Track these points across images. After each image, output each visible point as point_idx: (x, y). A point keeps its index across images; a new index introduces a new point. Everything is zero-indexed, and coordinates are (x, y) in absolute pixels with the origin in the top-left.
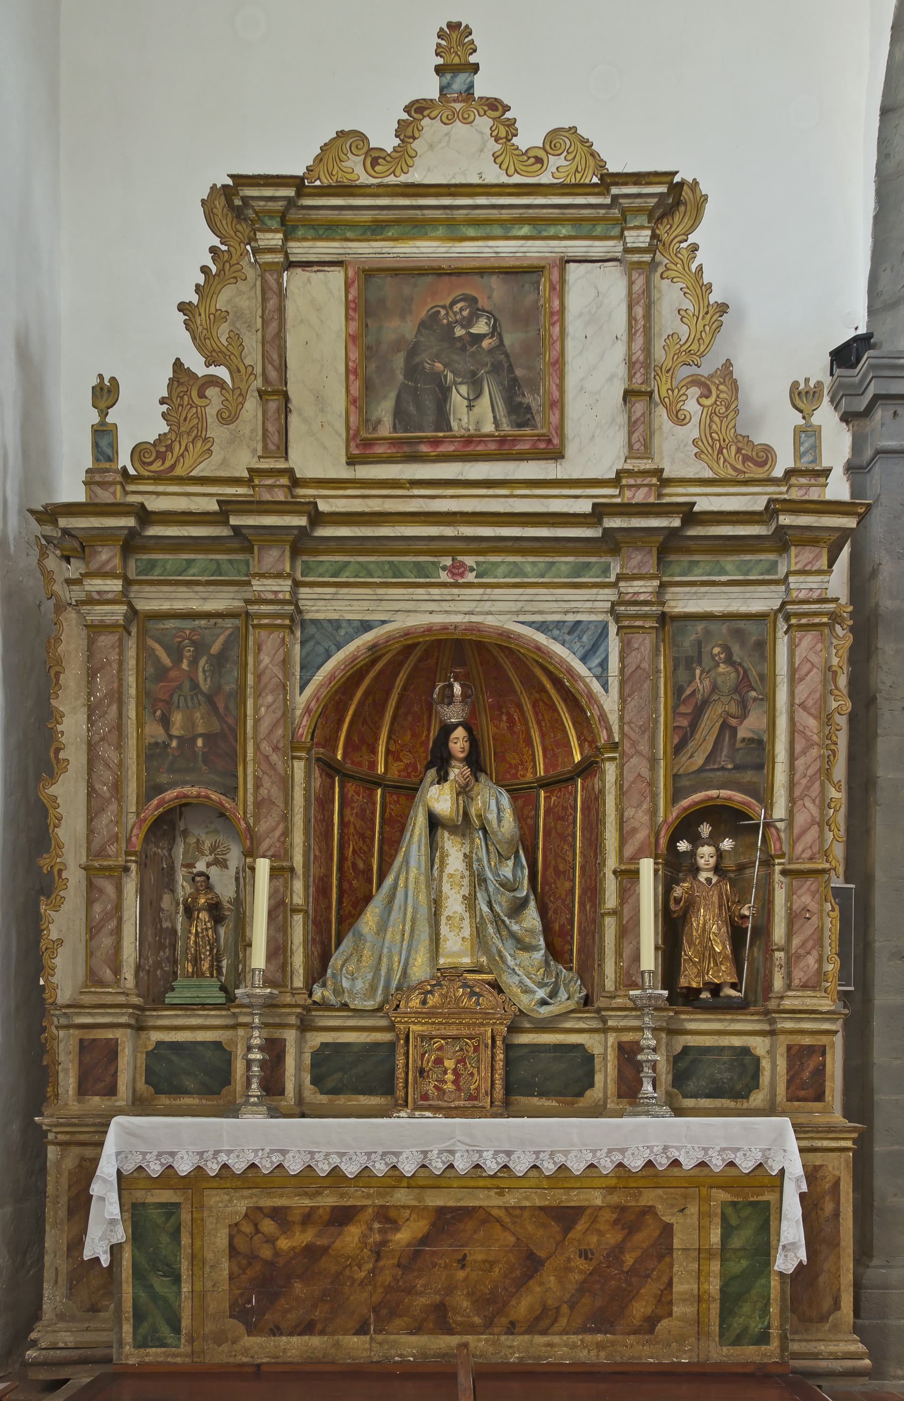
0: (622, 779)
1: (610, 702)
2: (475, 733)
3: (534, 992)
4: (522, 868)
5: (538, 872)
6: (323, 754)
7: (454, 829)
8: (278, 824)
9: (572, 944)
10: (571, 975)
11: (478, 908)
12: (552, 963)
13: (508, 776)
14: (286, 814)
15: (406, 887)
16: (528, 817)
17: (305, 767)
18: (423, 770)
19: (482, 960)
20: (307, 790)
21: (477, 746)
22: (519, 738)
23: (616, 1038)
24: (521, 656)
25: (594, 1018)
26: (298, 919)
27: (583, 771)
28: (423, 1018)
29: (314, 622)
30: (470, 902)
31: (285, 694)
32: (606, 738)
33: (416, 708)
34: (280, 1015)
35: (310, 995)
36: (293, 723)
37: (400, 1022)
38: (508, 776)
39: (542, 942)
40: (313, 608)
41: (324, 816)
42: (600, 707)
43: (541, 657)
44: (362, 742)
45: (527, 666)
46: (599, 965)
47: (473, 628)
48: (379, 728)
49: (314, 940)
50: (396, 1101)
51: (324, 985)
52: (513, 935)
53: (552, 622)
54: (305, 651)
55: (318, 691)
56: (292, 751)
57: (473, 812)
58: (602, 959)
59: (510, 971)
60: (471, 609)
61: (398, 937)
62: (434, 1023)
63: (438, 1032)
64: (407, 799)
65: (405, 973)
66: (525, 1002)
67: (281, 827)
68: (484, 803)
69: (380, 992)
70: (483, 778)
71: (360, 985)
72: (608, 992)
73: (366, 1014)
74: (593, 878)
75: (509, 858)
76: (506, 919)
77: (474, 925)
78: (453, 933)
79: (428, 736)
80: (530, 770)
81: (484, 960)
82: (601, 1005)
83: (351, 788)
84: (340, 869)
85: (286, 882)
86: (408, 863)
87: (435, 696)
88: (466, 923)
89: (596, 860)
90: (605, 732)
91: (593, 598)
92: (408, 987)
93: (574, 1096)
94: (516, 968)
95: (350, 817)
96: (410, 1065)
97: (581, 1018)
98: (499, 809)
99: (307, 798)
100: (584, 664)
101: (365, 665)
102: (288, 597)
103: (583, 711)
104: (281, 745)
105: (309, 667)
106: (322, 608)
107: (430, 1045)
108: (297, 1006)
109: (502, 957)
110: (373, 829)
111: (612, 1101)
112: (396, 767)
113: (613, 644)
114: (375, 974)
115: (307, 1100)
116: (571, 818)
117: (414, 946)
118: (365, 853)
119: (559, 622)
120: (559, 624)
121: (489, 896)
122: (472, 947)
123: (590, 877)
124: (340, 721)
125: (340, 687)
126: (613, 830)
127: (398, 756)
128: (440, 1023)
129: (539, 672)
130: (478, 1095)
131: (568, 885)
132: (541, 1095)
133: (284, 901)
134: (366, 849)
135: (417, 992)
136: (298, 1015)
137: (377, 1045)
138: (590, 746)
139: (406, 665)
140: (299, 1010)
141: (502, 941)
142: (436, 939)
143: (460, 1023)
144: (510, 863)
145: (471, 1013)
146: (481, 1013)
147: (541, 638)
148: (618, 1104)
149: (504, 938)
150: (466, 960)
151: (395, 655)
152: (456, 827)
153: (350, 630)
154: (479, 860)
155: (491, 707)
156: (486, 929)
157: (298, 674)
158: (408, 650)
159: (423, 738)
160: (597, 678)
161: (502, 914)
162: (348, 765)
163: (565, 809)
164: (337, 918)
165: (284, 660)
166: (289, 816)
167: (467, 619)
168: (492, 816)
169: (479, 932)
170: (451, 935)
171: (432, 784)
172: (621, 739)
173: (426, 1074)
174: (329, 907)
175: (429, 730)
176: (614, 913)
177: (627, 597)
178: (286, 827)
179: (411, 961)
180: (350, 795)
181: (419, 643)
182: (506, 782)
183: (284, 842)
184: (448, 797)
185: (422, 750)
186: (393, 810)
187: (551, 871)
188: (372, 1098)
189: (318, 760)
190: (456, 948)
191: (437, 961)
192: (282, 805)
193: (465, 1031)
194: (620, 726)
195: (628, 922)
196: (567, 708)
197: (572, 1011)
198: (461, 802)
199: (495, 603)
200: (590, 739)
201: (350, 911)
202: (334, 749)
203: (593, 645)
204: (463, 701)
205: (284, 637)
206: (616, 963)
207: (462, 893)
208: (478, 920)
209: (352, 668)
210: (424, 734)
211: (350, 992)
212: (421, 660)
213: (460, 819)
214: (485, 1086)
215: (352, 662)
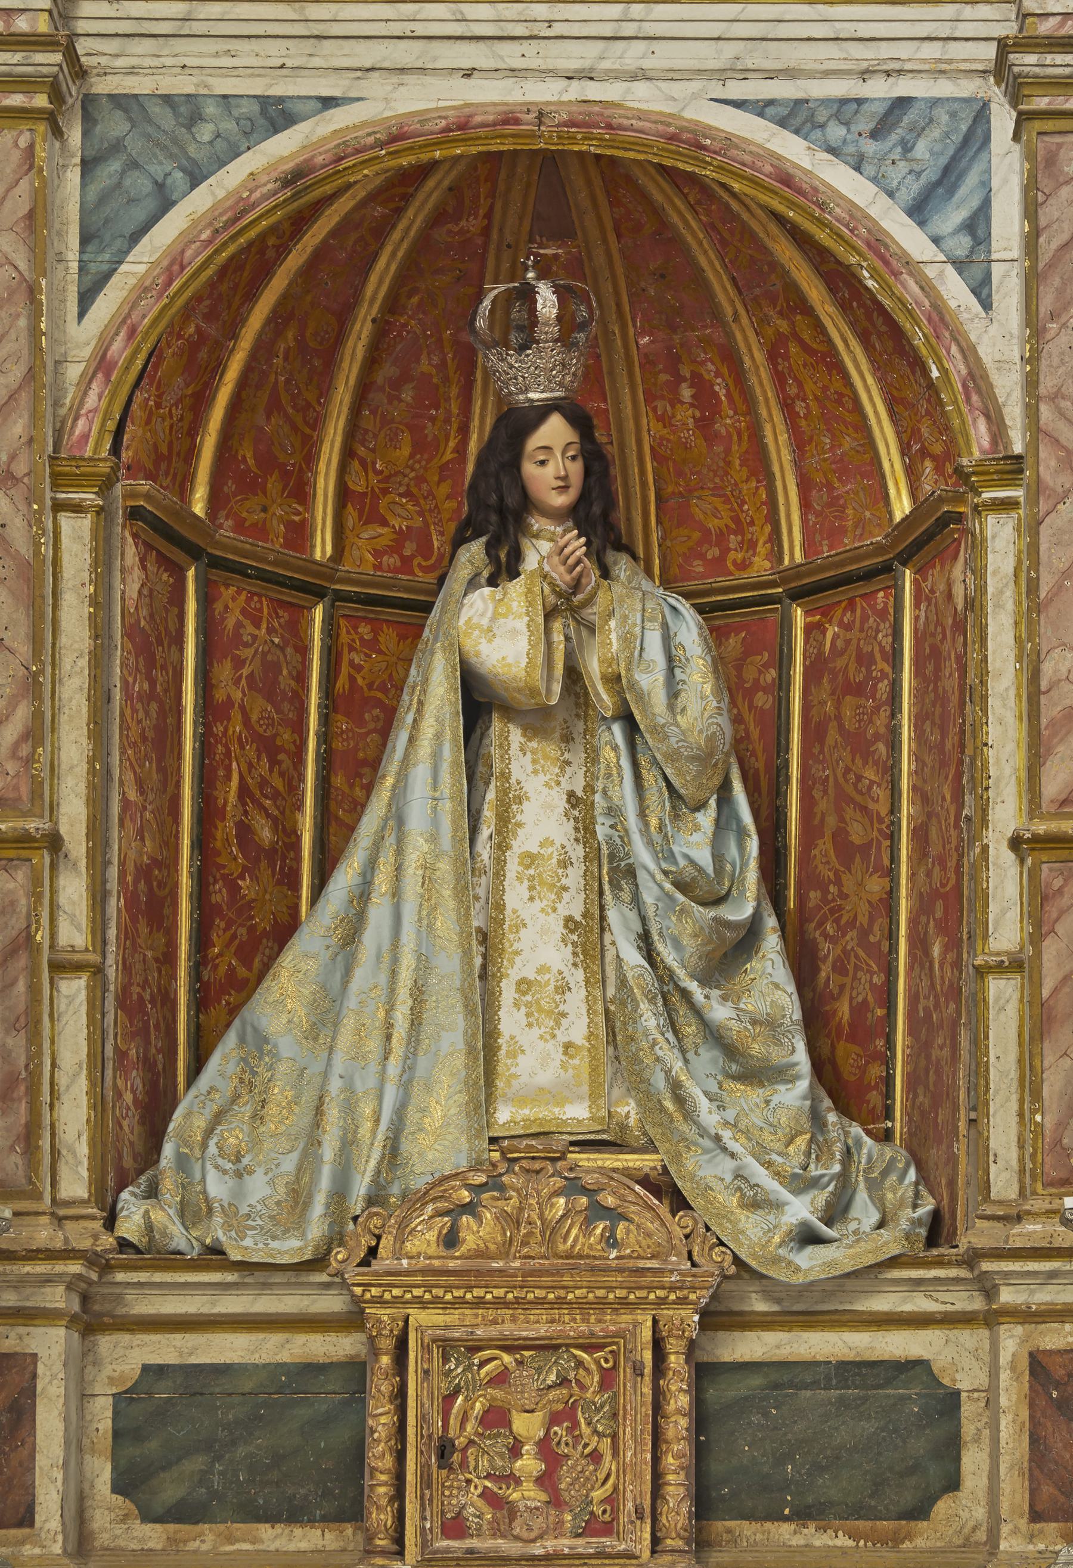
0: (1035, 563)
1: (997, 338)
2: (600, 436)
3: (778, 1206)
4: (742, 834)
5: (786, 847)
6: (147, 497)
7: (536, 720)
8: (13, 704)
9: (889, 1063)
10: (888, 1153)
11: (610, 955)
12: (832, 1117)
13: (698, 567)
14: (35, 675)
15: (396, 893)
16: (757, 686)
17: (95, 537)
18: (448, 548)
19: (622, 1110)
20: (100, 602)
21: (605, 473)
22: (728, 451)
23: (1024, 1341)
24: (735, 205)
25: (957, 1280)
26: (74, 989)
27: (918, 545)
28: (449, 1288)
29: (118, 101)
30: (588, 936)
31: (36, 315)
32: (986, 443)
33: (425, 366)
34: (20, 1283)
35: (110, 1222)
36: (57, 404)
37: (379, 1301)
38: (698, 567)
39: (801, 1057)
40: (120, 62)
41: (153, 683)
42: (969, 352)
43: (792, 205)
44: (263, 467)
45: (753, 236)
46: (972, 1122)
47: (588, 119)
48: (317, 423)
49: (121, 1055)
50: (370, 1539)
51: (152, 1192)
52: (714, 1035)
53: (825, 102)
54: (94, 191)
55: (134, 306)
56: (55, 486)
57: (593, 667)
58: (980, 1105)
59: (707, 1143)
60: (586, 64)
61: (374, 1045)
62: (479, 1303)
63: (493, 1331)
64: (402, 637)
65: (393, 1153)
66: (752, 1234)
67: (22, 713)
68: (626, 639)
69: (318, 1208)
70: (622, 566)
71: (259, 1189)
72: (1000, 1202)
73: (278, 1278)
74: (951, 864)
75: (700, 806)
76: (693, 986)
77: (599, 1007)
78: (536, 1031)
79: (461, 450)
80: (762, 549)
81: (629, 1109)
82: (980, 1242)
83: (233, 600)
84: (202, 843)
85: (36, 881)
86: (401, 822)
87: (481, 323)
88: (576, 1001)
89: (961, 806)
90: (982, 425)
91: (945, 31)
92: (404, 1196)
93: (900, 1518)
94: (726, 1135)
95: (229, 686)
96: (411, 1431)
97: (919, 1282)
98: (670, 659)
99: (99, 629)
100: (921, 224)
101: (273, 229)
102: (43, 25)
103: (918, 365)
104: (20, 468)
105: (106, 236)
106: (148, 62)
107: (468, 1368)
108: (68, 1254)
109: (680, 1100)
110: (300, 727)
111: (1015, 1531)
112: (367, 539)
113: (1005, 164)
114: (304, 1155)
115: (103, 1539)
116: (883, 686)
117: (420, 1072)
118: (276, 795)
119: (844, 102)
120: (845, 108)
121: (643, 919)
122: (594, 1070)
123: (942, 861)
124: (201, 402)
125: (198, 298)
126: (1010, 719)
127: (374, 507)
128: (500, 1303)
129: (785, 252)
130: (615, 1518)
131: (876, 885)
132: (802, 1515)
133: (30, 938)
134: (278, 783)
135: (430, 1209)
136: (72, 1283)
137: (311, 1370)
138: (939, 469)
139: (396, 235)
140: (75, 1268)
141: (683, 1052)
142: (486, 1050)
143: (560, 1302)
144: (706, 819)
145: (592, 1270)
146: (621, 1270)
147: (792, 149)
148: (1031, 1538)
149: (688, 1043)
150: (577, 1113)
151: (362, 204)
152: (545, 712)
153: (229, 126)
154: (613, 811)
155: (648, 362)
156: (634, 1017)
157: (73, 256)
158: (405, 183)
159: (449, 455)
160: (960, 265)
161: (680, 973)
162: (226, 532)
163: (864, 660)
164: (192, 991)
165: (31, 215)
166: (46, 680)
167: (575, 91)
168: (651, 680)
169: (614, 1027)
170: (529, 1038)
171: (472, 584)
172: (1033, 445)
173: (456, 1457)
174: (169, 958)
175: (464, 431)
176: (1014, 965)
177: (1045, 28)
178: (37, 715)
179: (412, 1116)
180: (230, 623)
181: (434, 164)
182: (692, 585)
183: (29, 761)
184: (521, 624)
185: (444, 489)
186: (359, 668)
187: (825, 846)
188: (298, 1531)
189: (134, 514)
190: (546, 1077)
191: (490, 1113)
192: (24, 649)
193: (574, 1326)
194: (1027, 406)
195: (1056, 990)
196: (872, 361)
197: (894, 1262)
198: (558, 638)
199: (656, 45)
200: (938, 449)
201: (231, 969)
202: (184, 486)
203: (947, 170)
204: (564, 339)
205: (31, 147)
206: (1021, 1115)
207: (563, 911)
208: (611, 991)
209: (234, 238)
210: (452, 444)
211: (231, 1211)
212: (438, 218)
213: (557, 688)
214: (636, 1491)
215: (236, 219)
